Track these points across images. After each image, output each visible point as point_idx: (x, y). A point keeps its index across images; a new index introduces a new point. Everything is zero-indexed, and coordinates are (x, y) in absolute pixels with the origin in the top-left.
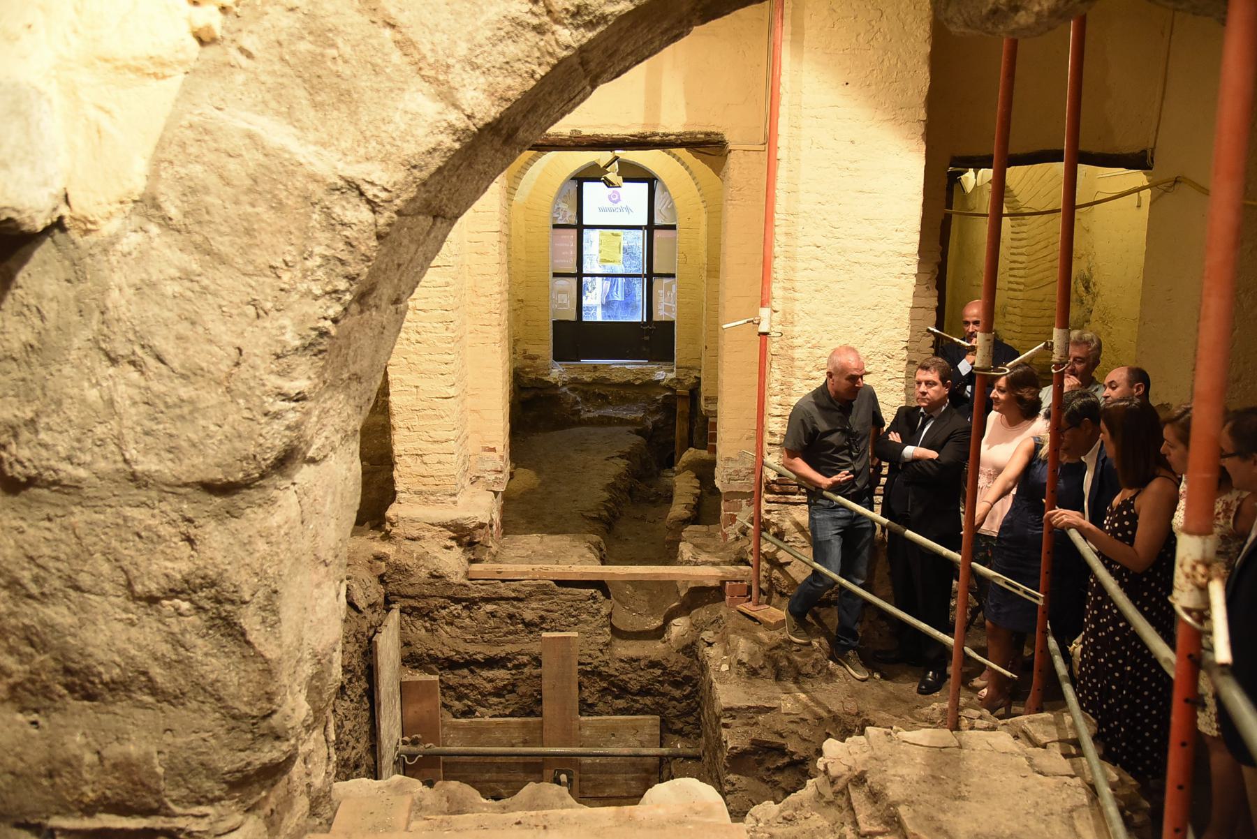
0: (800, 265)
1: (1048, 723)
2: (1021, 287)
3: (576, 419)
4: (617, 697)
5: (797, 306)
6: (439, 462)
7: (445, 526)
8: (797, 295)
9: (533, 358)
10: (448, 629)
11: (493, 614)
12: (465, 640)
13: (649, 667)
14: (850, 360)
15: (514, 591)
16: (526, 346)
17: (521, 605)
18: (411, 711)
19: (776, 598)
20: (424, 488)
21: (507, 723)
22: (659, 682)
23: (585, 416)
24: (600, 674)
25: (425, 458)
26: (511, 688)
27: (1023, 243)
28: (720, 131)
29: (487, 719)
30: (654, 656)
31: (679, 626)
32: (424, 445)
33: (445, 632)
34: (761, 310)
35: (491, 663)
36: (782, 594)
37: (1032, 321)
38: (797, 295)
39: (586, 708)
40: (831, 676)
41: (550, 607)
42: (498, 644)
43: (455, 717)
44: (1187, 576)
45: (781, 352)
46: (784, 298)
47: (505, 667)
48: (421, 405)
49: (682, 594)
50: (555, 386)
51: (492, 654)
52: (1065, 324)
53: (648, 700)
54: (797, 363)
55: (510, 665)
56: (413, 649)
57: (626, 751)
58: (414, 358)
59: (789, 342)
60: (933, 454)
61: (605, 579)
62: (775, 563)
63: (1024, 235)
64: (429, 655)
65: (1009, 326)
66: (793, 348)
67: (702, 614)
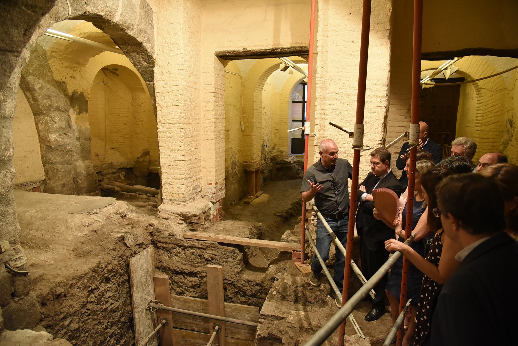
0: (328, 102)
2: (480, 125)
4: (243, 296)
8: (327, 117)
9: (282, 152)
10: (176, 257)
11: (193, 254)
13: (256, 285)
15: (201, 245)
16: (279, 147)
18: (158, 289)
20: (173, 198)
21: (195, 300)
22: (259, 292)
24: (234, 285)
25: (173, 186)
26: (198, 286)
27: (481, 105)
28: (307, 45)
29: (188, 297)
32: (173, 180)
33: (175, 258)
35: (191, 274)
37: (485, 140)
38: (327, 117)
39: (226, 299)
41: (215, 253)
42: (195, 266)
43: (177, 294)
46: (320, 118)
47: (196, 276)
50: (290, 163)
51: (191, 270)
53: (254, 300)
55: (198, 276)
56: (162, 264)
57: (238, 321)
61: (244, 244)
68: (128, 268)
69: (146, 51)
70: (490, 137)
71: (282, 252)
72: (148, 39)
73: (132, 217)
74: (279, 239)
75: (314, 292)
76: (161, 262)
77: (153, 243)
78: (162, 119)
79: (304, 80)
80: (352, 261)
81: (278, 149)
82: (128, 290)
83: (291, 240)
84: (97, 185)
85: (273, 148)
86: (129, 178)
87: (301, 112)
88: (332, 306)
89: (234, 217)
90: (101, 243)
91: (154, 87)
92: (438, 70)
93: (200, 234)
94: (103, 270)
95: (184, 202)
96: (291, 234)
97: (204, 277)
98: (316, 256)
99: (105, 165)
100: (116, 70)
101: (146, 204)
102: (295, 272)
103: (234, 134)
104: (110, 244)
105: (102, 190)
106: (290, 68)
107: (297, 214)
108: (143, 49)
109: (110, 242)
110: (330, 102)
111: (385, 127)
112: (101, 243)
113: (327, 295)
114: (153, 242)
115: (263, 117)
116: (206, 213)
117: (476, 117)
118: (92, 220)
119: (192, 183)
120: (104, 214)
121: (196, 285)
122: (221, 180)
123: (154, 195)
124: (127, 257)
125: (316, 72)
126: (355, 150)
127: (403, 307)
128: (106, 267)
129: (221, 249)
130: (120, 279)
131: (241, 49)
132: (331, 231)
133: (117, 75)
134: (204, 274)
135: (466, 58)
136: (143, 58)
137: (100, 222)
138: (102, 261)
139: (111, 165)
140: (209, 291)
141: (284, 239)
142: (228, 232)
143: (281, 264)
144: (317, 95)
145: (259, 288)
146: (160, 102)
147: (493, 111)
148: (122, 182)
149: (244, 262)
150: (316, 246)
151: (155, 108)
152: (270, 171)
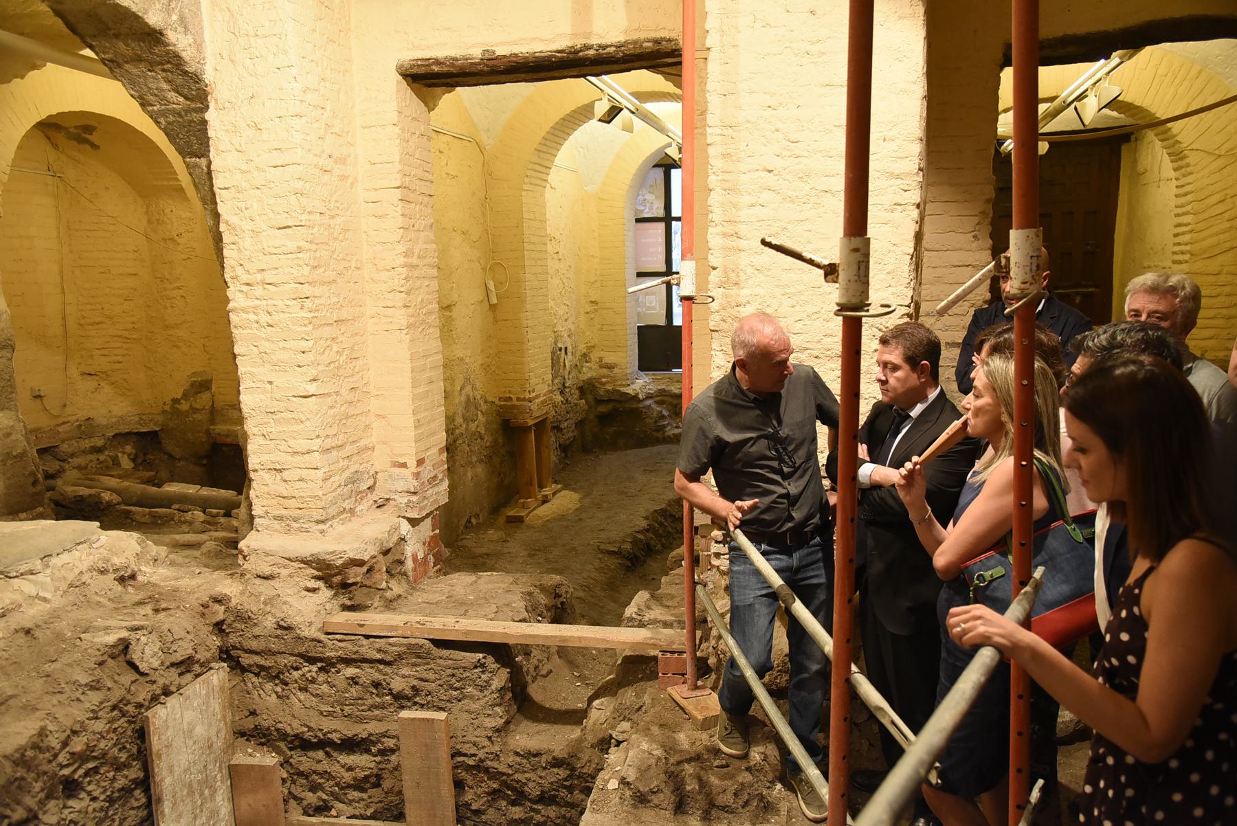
0: (746, 199)
2: (1187, 257)
3: (659, 435)
4: (514, 803)
6: (301, 480)
7: (306, 562)
9: (610, 367)
10: (302, 696)
11: (354, 681)
12: (321, 713)
13: (553, 766)
14: (765, 334)
15: (379, 651)
16: (602, 354)
17: (388, 670)
18: (245, 802)
20: (285, 512)
22: (565, 787)
24: (487, 770)
25: (285, 474)
27: (1189, 198)
28: (673, 35)
33: (298, 699)
35: (351, 745)
41: (425, 675)
42: (360, 720)
43: (306, 813)
46: (725, 248)
47: (368, 751)
48: (277, 406)
50: (635, 398)
51: (350, 734)
56: (258, 720)
58: (265, 346)
61: (511, 642)
64: (277, 730)
68: (143, 741)
69: (178, 57)
70: (1219, 290)
71: (629, 660)
72: (182, 19)
73: (154, 579)
74: (617, 620)
75: (731, 777)
76: (253, 713)
77: (227, 655)
78: (239, 271)
79: (669, 151)
80: (854, 668)
81: (601, 359)
82: (143, 813)
83: (654, 622)
84: (39, 488)
85: (585, 355)
86: (148, 465)
87: (662, 249)
88: (789, 817)
89: (477, 563)
90: (48, 667)
91: (209, 173)
92: (1057, 102)
93: (375, 619)
94: (56, 756)
95: (323, 522)
96: (653, 603)
97: (393, 751)
98: (733, 663)
99: (66, 427)
100: (89, 129)
101: (204, 537)
102: (669, 717)
103: (469, 314)
104: (78, 670)
105: (57, 504)
106: (625, 112)
107: (663, 546)
108: (168, 52)
109: (78, 663)
111: (917, 265)
112: (48, 667)
113: (772, 782)
114: (227, 652)
115: (552, 265)
116: (391, 554)
117: (1176, 235)
118: (17, 597)
119: (342, 464)
120: (57, 574)
121: (366, 777)
122: (435, 450)
123: (229, 509)
124: (140, 706)
125: (703, 113)
126: (845, 318)
127: (1021, 808)
128: (65, 744)
129: (440, 661)
130: (114, 779)
131: (476, 53)
132: (777, 581)
133: (94, 146)
134: (390, 743)
135: (1150, 53)
136: (169, 81)
137: (45, 600)
138: (51, 727)
139: (86, 427)
140: (408, 794)
141: (631, 619)
142: (463, 607)
143: (628, 696)
144: (712, 180)
145: (562, 773)
146: (234, 220)
147: (1226, 216)
148: (125, 476)
149: (515, 697)
150: (732, 632)
151: (218, 238)
152: (580, 424)
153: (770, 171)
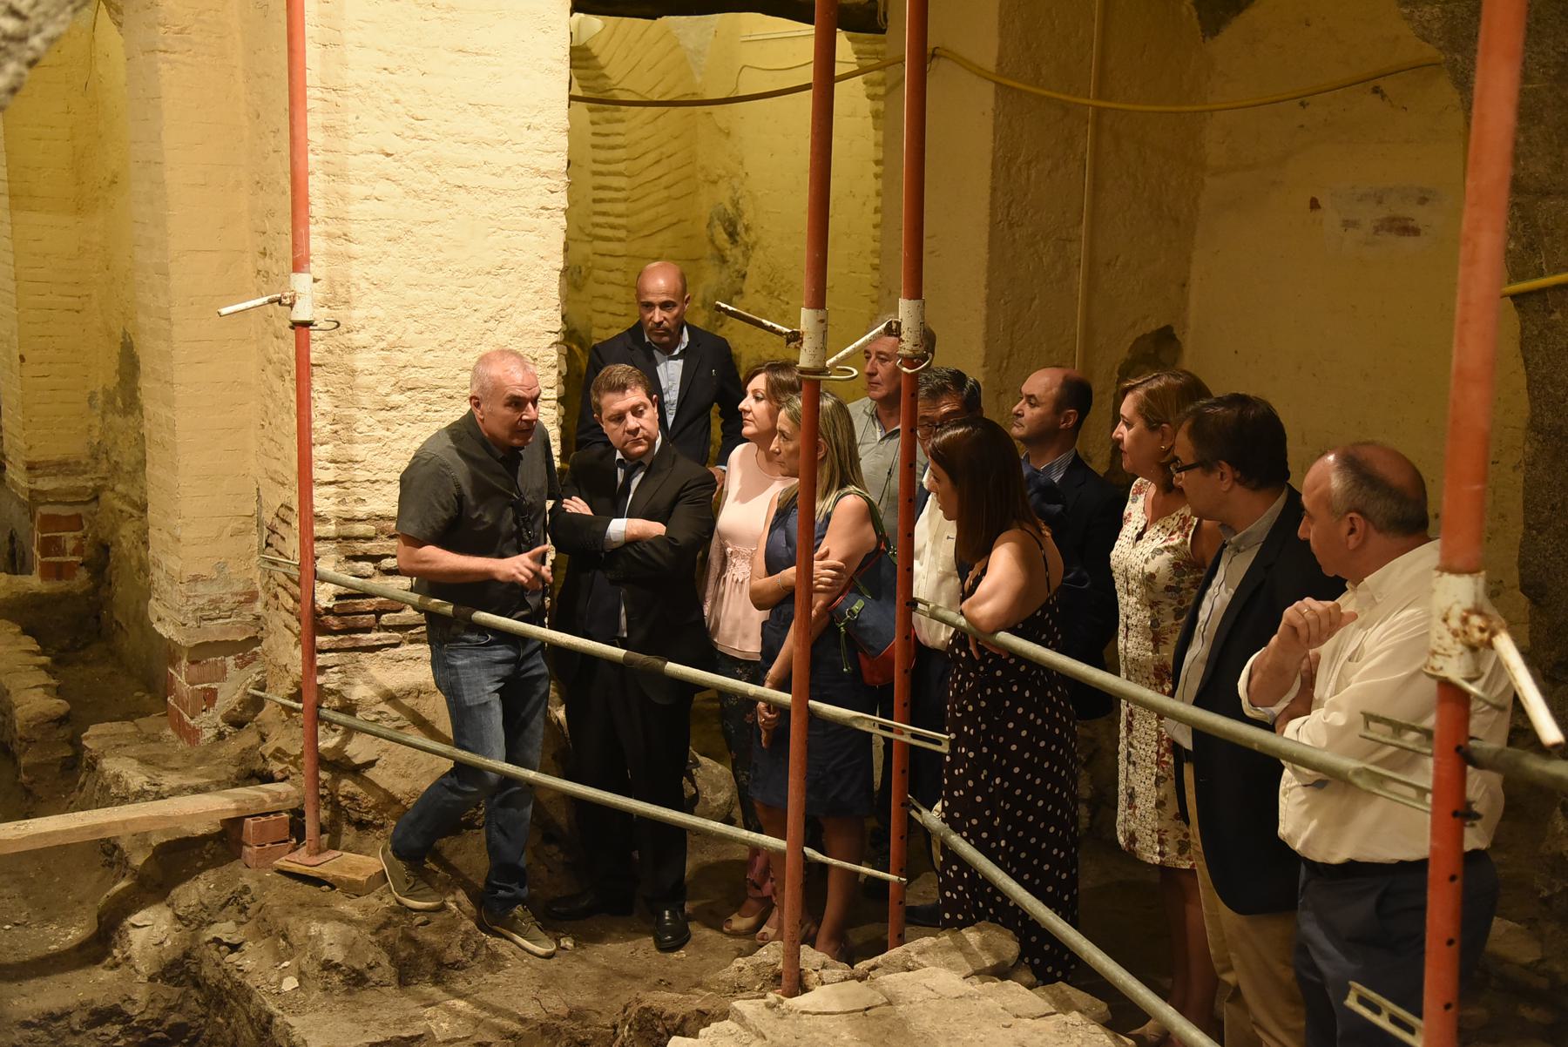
0: (357, 190)
1: (950, 949)
5: (356, 270)
8: (354, 248)
13: (91, 1025)
19: (349, 835)
23: (406, 582)
27: (619, 153)
30: (101, 1000)
31: (150, 931)
34: (294, 276)
36: (361, 825)
38: (354, 248)
40: (494, 961)
44: (1455, 634)
45: (330, 359)
46: (330, 254)
49: (138, 860)
52: (916, 292)
54: (362, 380)
59: (343, 340)
60: (658, 528)
62: (339, 765)
63: (619, 140)
65: (600, 305)
66: (351, 350)
67: (196, 891)
110: (366, 191)
147: (664, 181)
153: (388, 155)
